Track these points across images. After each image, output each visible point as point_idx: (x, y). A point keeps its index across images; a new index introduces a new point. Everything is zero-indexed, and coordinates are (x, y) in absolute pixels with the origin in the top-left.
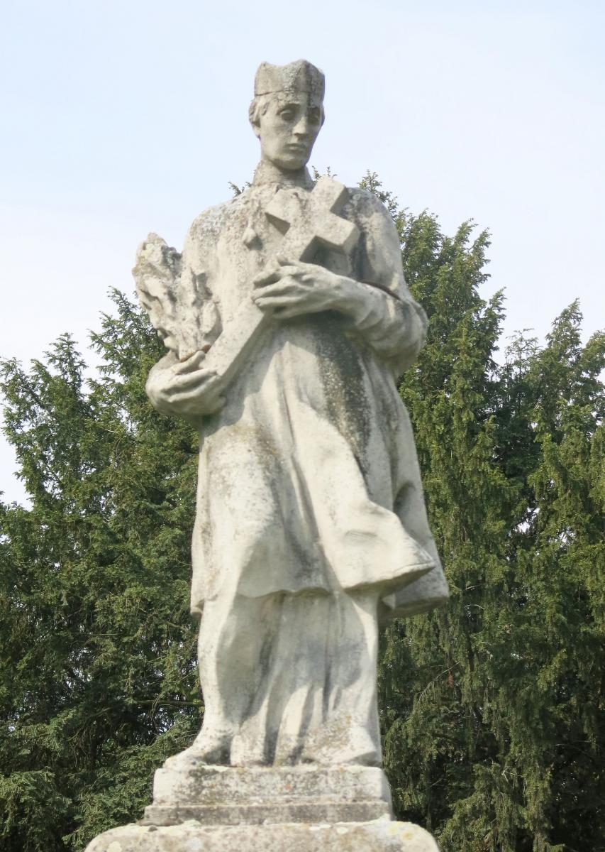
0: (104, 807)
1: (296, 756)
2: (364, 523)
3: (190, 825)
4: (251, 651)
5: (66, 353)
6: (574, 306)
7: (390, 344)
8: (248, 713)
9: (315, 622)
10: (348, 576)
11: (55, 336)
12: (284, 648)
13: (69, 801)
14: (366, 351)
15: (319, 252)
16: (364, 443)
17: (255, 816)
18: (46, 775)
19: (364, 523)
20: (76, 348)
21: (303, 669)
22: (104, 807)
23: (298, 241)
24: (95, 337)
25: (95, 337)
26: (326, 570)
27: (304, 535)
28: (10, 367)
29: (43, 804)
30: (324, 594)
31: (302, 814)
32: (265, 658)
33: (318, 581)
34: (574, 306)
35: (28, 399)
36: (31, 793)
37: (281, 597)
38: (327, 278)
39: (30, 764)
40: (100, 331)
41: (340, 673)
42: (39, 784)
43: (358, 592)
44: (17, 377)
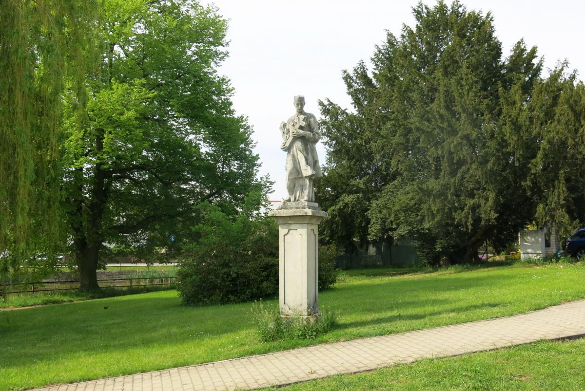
0: (377, 204)
1: (298, 200)
2: (306, 168)
3: (283, 210)
4: (292, 186)
5: (362, 66)
6: (522, 40)
7: (312, 140)
8: (292, 194)
9: (301, 182)
10: (304, 175)
11: (358, 61)
12: (296, 185)
13: (368, 203)
14: (309, 141)
15: (301, 128)
16: (308, 153)
17: (291, 208)
18: (361, 195)
19: (306, 168)
20: (365, 64)
21: (299, 188)
22: (377, 204)
23: (298, 126)
24: (372, 59)
25: (372, 59)
26: (302, 174)
27: (299, 169)
28: (345, 72)
29: (360, 204)
30: (302, 177)
31: (297, 208)
32: (294, 187)
33: (300, 176)
34: (522, 40)
35: (351, 81)
36: (355, 201)
37: (296, 178)
38: (301, 131)
39: (357, 192)
40: (373, 57)
41: (304, 189)
42: (358, 198)
43: (306, 177)
44: (347, 75)
